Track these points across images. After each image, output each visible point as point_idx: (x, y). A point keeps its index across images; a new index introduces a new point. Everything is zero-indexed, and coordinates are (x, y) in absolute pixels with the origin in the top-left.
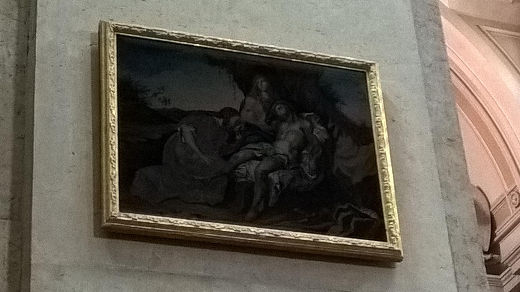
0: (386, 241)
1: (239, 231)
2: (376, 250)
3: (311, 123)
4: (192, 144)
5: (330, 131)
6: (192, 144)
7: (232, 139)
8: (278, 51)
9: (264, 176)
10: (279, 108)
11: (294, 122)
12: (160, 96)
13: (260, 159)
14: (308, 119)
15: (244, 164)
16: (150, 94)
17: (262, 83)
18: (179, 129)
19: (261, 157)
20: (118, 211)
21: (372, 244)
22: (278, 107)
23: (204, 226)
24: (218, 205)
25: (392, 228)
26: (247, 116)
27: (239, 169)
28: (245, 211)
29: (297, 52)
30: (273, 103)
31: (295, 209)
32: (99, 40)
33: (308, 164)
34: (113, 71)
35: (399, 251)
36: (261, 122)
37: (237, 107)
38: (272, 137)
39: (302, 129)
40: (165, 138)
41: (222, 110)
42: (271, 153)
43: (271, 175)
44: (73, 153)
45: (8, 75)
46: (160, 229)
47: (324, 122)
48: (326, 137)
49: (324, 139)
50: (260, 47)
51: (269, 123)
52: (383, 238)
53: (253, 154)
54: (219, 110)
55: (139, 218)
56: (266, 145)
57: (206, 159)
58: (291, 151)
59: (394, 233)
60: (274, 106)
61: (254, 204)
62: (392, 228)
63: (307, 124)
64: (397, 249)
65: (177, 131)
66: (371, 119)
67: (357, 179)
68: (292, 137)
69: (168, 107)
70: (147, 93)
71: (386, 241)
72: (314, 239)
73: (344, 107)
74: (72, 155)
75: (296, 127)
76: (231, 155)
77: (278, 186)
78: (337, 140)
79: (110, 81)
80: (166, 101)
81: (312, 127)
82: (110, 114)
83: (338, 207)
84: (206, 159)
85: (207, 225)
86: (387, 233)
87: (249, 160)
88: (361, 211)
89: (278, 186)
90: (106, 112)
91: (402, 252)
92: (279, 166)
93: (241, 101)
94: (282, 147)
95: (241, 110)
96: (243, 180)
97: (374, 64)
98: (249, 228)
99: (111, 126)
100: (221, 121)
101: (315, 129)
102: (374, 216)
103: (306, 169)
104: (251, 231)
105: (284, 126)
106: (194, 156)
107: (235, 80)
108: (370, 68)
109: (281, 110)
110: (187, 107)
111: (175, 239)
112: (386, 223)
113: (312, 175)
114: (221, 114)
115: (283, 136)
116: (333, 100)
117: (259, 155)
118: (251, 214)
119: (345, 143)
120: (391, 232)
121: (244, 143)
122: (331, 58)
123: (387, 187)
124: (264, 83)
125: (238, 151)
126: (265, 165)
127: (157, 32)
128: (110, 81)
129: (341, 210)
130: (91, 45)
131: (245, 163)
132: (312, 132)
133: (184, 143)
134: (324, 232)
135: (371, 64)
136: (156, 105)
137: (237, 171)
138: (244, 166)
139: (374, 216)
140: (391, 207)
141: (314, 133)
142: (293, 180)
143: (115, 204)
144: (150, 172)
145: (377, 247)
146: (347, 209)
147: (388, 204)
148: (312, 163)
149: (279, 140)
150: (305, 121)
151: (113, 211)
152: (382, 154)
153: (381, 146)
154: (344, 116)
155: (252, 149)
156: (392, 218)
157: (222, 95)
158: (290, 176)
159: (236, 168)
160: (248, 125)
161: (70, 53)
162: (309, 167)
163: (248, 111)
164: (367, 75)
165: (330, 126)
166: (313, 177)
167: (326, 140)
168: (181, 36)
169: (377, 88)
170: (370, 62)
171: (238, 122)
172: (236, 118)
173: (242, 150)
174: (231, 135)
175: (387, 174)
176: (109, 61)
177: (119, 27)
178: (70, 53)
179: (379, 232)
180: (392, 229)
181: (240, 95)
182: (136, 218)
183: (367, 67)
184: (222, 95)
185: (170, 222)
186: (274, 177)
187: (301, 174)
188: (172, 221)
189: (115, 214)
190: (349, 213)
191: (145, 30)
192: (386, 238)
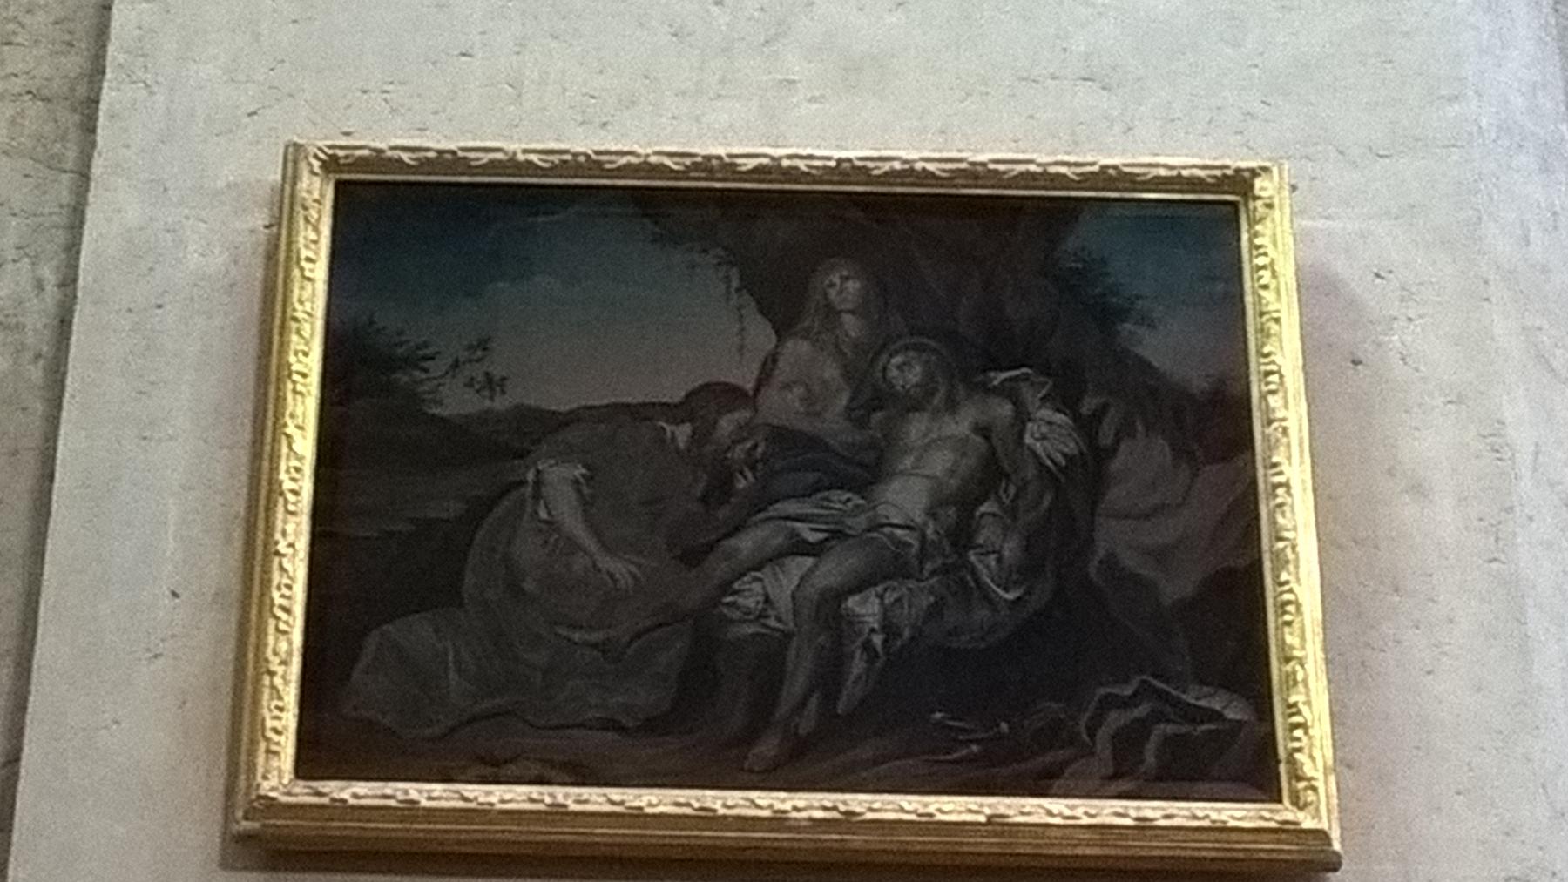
0: (1280, 801)
1: (931, 815)
2: (1234, 836)
3: (1018, 403)
4: (574, 525)
5: (1087, 426)
6: (574, 525)
7: (721, 487)
8: (1039, 170)
9: (829, 610)
10: (899, 367)
11: (952, 406)
12: (467, 371)
13: (815, 550)
14: (1009, 392)
15: (758, 574)
16: (438, 368)
17: (843, 286)
18: (530, 476)
19: (822, 542)
20: (288, 777)
21: (1214, 816)
22: (897, 360)
23: (586, 802)
24: (652, 726)
25: (1299, 750)
26: (782, 406)
27: (736, 592)
28: (750, 737)
29: (973, 164)
30: (878, 354)
31: (938, 715)
32: (284, 208)
33: (997, 547)
34: (308, 306)
35: (1322, 836)
36: (833, 423)
37: (746, 378)
38: (867, 471)
39: (984, 431)
40: (479, 510)
41: (689, 395)
42: (861, 521)
43: (852, 602)
44: (175, 595)
45: (29, 355)
46: (638, 831)
47: (1066, 399)
48: (1071, 448)
49: (1065, 455)
50: (840, 161)
51: (861, 423)
52: (1271, 793)
53: (794, 534)
54: (678, 396)
55: (940, 810)
56: (840, 499)
57: (620, 569)
58: (931, 513)
59: (1308, 770)
60: (884, 357)
61: (783, 709)
62: (1299, 750)
63: (1004, 410)
64: (1308, 823)
65: (523, 483)
66: (1248, 368)
67: (1177, 586)
68: (940, 462)
69: (501, 404)
70: (426, 364)
71: (1280, 801)
72: (990, 818)
73: (1142, 331)
74: (167, 601)
75: (960, 425)
76: (711, 547)
77: (877, 640)
78: (1112, 451)
79: (294, 338)
80: (492, 384)
81: (1022, 417)
82: (285, 450)
83: (1102, 691)
84: (620, 569)
85: (596, 799)
86: (1283, 768)
87: (777, 557)
88: (1189, 698)
89: (877, 640)
90: (274, 440)
91: (1335, 835)
92: (890, 566)
93: (762, 355)
94: (905, 499)
95: (757, 390)
96: (751, 629)
97: (1265, 169)
98: (754, 795)
99: (282, 494)
100: (683, 433)
101: (1030, 425)
102: (1235, 711)
103: (985, 568)
104: (759, 807)
105: (917, 428)
106: (579, 563)
107: (747, 285)
108: (1252, 186)
109: (905, 371)
110: (560, 400)
111: (900, 866)
112: (1280, 733)
113: (1006, 589)
114: (690, 407)
115: (908, 462)
116: (1108, 315)
117: (813, 537)
118: (768, 747)
119: (1141, 462)
120: (1292, 761)
121: (761, 501)
122: (1104, 168)
123: (1289, 602)
124: (853, 286)
125: (736, 530)
126: (832, 571)
127: (472, 155)
128: (294, 338)
129: (1109, 703)
130: (266, 227)
131: (758, 569)
132: (1021, 435)
133: (546, 522)
134: (1039, 786)
135: (1254, 173)
136: (456, 401)
137: (729, 599)
138: (760, 580)
139: (1235, 711)
140: (1300, 677)
141: (1028, 440)
142: (935, 611)
143: (276, 753)
144: (417, 633)
145: (1232, 823)
146: (1135, 694)
147: (1288, 668)
148: (1011, 548)
149: (892, 475)
150: (994, 401)
151: (265, 778)
152: (1276, 486)
153: (1275, 459)
154: (1145, 366)
155: (787, 518)
156: (1299, 713)
157: (697, 339)
158: (926, 600)
159: (726, 587)
160: (781, 437)
161: (194, 260)
162: (999, 561)
163: (787, 386)
164: (1242, 209)
165: (1088, 405)
166: (1010, 596)
167: (1069, 458)
168: (555, 158)
169: (1275, 251)
170: (1253, 164)
171: (746, 430)
172: (742, 415)
173: (756, 524)
174: (711, 477)
175: (1291, 556)
176: (296, 272)
177: (341, 153)
178: (194, 260)
179: (1256, 767)
180: (1297, 756)
181: (761, 335)
182: (931, 809)
183: (1242, 182)
184: (697, 339)
185: (466, 799)
186: (867, 608)
187: (964, 587)
188: (471, 795)
189: (273, 789)
190: (1141, 711)
191: (431, 155)
192: (1279, 791)
